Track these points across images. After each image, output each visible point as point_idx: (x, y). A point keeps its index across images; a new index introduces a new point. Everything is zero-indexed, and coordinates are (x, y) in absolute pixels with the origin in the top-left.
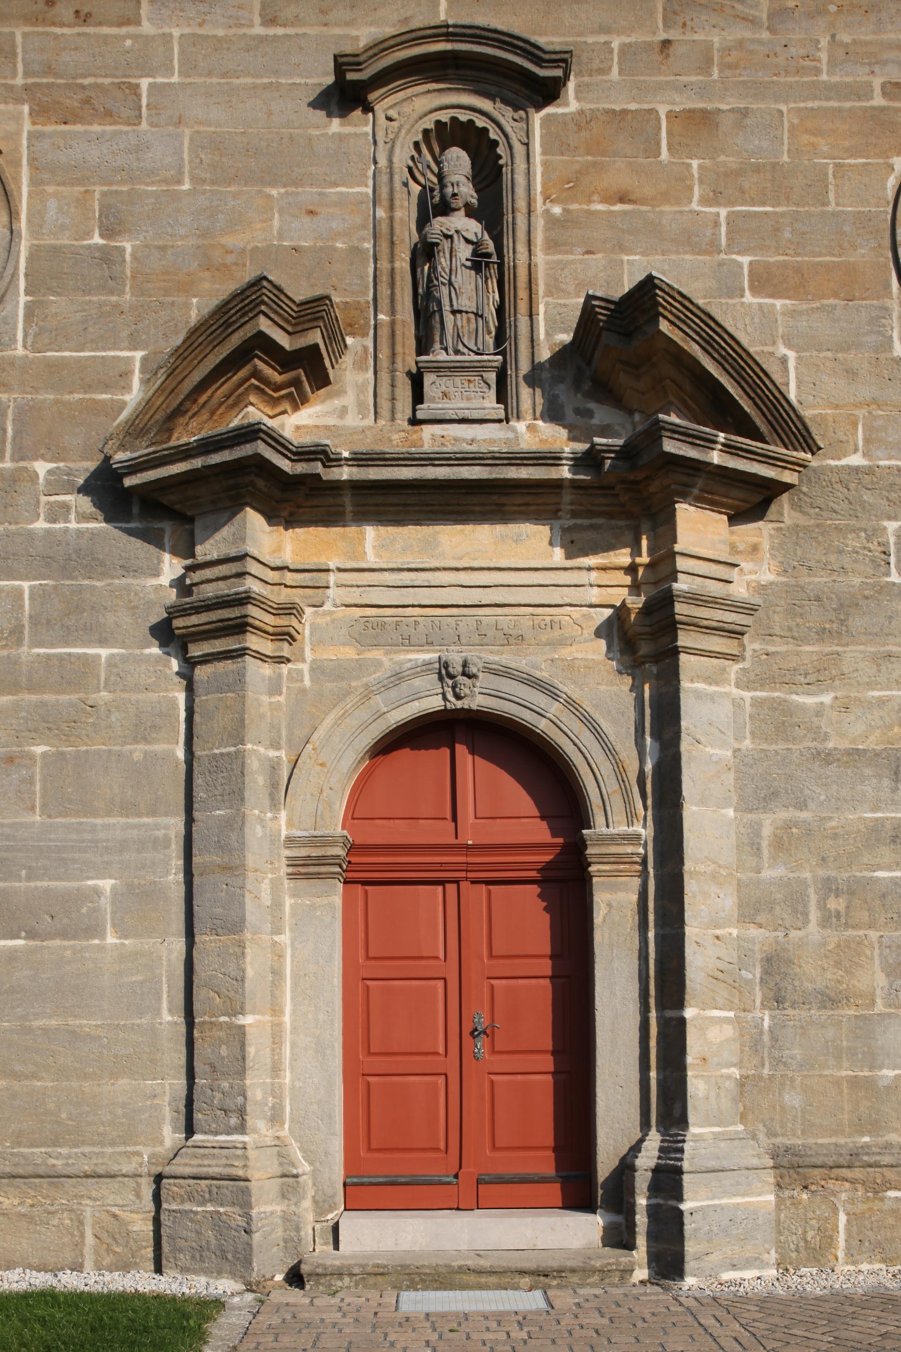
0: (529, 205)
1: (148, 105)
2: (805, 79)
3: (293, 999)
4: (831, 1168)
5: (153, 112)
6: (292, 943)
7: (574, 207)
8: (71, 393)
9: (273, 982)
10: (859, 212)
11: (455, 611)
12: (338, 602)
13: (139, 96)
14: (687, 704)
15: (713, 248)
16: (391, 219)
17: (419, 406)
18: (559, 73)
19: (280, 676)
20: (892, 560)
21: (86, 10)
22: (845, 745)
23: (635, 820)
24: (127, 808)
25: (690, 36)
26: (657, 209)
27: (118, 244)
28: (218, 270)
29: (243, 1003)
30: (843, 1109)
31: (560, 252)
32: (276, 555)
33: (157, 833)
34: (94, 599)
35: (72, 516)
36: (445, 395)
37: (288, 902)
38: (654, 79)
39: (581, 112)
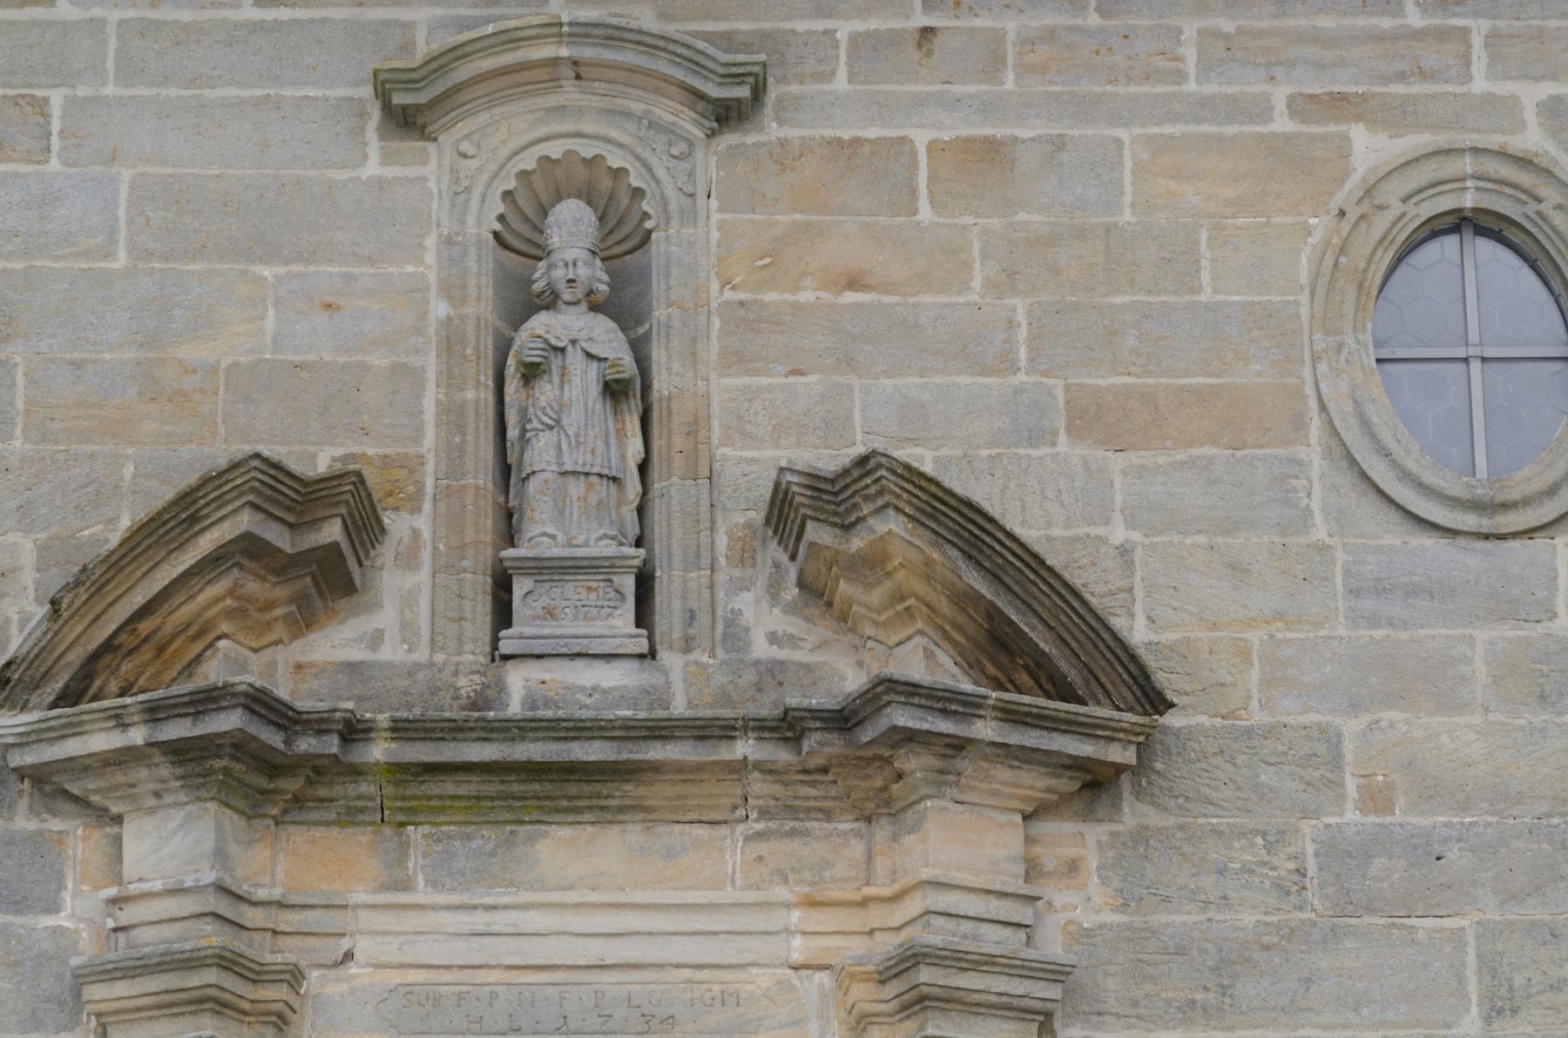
10: (1252, 304)
11: (559, 976)
13: (46, 116)
17: (502, 633)
18: (744, 92)
31: (747, 373)
38: (908, 88)
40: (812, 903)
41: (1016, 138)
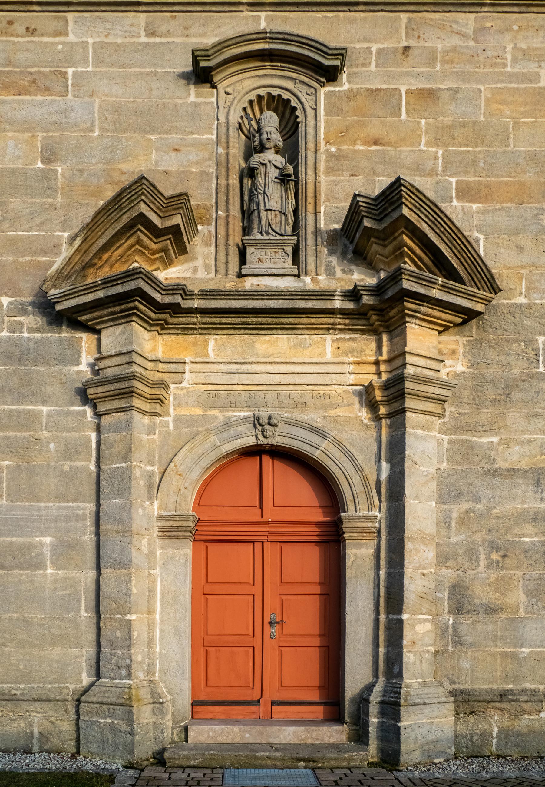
0: (316, 145)
1: (72, 84)
2: (496, 70)
3: (161, 605)
4: (489, 702)
5: (76, 88)
6: (161, 574)
7: (345, 147)
8: (23, 256)
9: (149, 596)
10: (528, 151)
11: (264, 388)
12: (191, 382)
13: (66, 79)
14: (409, 441)
15: (433, 172)
16: (227, 154)
17: (243, 267)
18: (337, 63)
19: (154, 424)
20: (541, 359)
21: (33, 27)
22: (506, 465)
23: (373, 508)
24: (60, 498)
25: (422, 44)
26: (398, 149)
27: (53, 168)
28: (116, 184)
29: (130, 608)
30: (497, 670)
31: (335, 175)
32: (152, 353)
33: (78, 511)
34: (39, 378)
35: (25, 330)
36: (260, 260)
37: (159, 552)
38: (399, 70)
39: (350, 90)
40: (358, 363)
41: (440, 89)
